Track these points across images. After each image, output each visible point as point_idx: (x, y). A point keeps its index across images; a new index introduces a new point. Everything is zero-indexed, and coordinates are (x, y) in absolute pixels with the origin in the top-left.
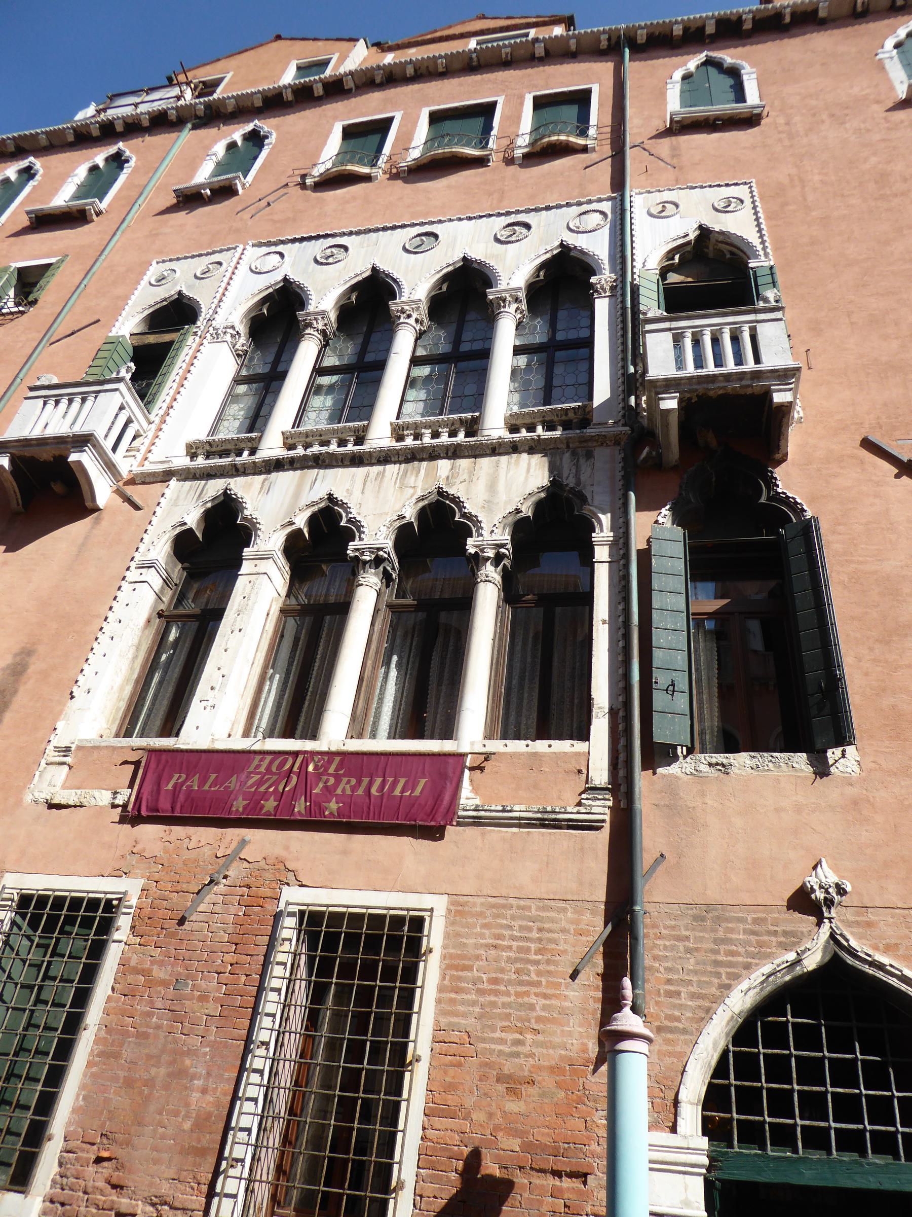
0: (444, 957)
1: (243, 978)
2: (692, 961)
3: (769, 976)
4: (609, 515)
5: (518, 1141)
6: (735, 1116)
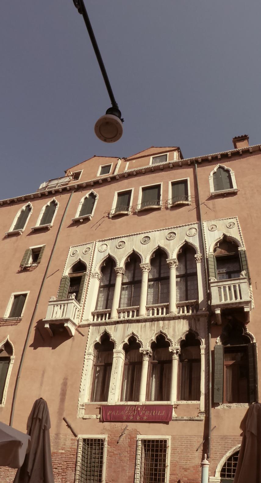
0: (171, 447)
1: (132, 453)
2: (220, 447)
3: (235, 449)
4: (204, 339)
5: (187, 479)
6: (226, 473)
